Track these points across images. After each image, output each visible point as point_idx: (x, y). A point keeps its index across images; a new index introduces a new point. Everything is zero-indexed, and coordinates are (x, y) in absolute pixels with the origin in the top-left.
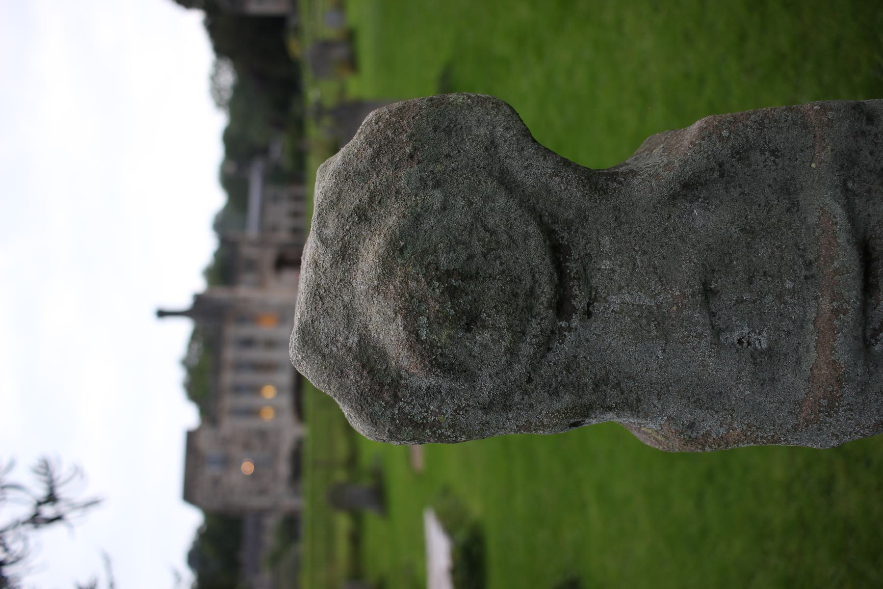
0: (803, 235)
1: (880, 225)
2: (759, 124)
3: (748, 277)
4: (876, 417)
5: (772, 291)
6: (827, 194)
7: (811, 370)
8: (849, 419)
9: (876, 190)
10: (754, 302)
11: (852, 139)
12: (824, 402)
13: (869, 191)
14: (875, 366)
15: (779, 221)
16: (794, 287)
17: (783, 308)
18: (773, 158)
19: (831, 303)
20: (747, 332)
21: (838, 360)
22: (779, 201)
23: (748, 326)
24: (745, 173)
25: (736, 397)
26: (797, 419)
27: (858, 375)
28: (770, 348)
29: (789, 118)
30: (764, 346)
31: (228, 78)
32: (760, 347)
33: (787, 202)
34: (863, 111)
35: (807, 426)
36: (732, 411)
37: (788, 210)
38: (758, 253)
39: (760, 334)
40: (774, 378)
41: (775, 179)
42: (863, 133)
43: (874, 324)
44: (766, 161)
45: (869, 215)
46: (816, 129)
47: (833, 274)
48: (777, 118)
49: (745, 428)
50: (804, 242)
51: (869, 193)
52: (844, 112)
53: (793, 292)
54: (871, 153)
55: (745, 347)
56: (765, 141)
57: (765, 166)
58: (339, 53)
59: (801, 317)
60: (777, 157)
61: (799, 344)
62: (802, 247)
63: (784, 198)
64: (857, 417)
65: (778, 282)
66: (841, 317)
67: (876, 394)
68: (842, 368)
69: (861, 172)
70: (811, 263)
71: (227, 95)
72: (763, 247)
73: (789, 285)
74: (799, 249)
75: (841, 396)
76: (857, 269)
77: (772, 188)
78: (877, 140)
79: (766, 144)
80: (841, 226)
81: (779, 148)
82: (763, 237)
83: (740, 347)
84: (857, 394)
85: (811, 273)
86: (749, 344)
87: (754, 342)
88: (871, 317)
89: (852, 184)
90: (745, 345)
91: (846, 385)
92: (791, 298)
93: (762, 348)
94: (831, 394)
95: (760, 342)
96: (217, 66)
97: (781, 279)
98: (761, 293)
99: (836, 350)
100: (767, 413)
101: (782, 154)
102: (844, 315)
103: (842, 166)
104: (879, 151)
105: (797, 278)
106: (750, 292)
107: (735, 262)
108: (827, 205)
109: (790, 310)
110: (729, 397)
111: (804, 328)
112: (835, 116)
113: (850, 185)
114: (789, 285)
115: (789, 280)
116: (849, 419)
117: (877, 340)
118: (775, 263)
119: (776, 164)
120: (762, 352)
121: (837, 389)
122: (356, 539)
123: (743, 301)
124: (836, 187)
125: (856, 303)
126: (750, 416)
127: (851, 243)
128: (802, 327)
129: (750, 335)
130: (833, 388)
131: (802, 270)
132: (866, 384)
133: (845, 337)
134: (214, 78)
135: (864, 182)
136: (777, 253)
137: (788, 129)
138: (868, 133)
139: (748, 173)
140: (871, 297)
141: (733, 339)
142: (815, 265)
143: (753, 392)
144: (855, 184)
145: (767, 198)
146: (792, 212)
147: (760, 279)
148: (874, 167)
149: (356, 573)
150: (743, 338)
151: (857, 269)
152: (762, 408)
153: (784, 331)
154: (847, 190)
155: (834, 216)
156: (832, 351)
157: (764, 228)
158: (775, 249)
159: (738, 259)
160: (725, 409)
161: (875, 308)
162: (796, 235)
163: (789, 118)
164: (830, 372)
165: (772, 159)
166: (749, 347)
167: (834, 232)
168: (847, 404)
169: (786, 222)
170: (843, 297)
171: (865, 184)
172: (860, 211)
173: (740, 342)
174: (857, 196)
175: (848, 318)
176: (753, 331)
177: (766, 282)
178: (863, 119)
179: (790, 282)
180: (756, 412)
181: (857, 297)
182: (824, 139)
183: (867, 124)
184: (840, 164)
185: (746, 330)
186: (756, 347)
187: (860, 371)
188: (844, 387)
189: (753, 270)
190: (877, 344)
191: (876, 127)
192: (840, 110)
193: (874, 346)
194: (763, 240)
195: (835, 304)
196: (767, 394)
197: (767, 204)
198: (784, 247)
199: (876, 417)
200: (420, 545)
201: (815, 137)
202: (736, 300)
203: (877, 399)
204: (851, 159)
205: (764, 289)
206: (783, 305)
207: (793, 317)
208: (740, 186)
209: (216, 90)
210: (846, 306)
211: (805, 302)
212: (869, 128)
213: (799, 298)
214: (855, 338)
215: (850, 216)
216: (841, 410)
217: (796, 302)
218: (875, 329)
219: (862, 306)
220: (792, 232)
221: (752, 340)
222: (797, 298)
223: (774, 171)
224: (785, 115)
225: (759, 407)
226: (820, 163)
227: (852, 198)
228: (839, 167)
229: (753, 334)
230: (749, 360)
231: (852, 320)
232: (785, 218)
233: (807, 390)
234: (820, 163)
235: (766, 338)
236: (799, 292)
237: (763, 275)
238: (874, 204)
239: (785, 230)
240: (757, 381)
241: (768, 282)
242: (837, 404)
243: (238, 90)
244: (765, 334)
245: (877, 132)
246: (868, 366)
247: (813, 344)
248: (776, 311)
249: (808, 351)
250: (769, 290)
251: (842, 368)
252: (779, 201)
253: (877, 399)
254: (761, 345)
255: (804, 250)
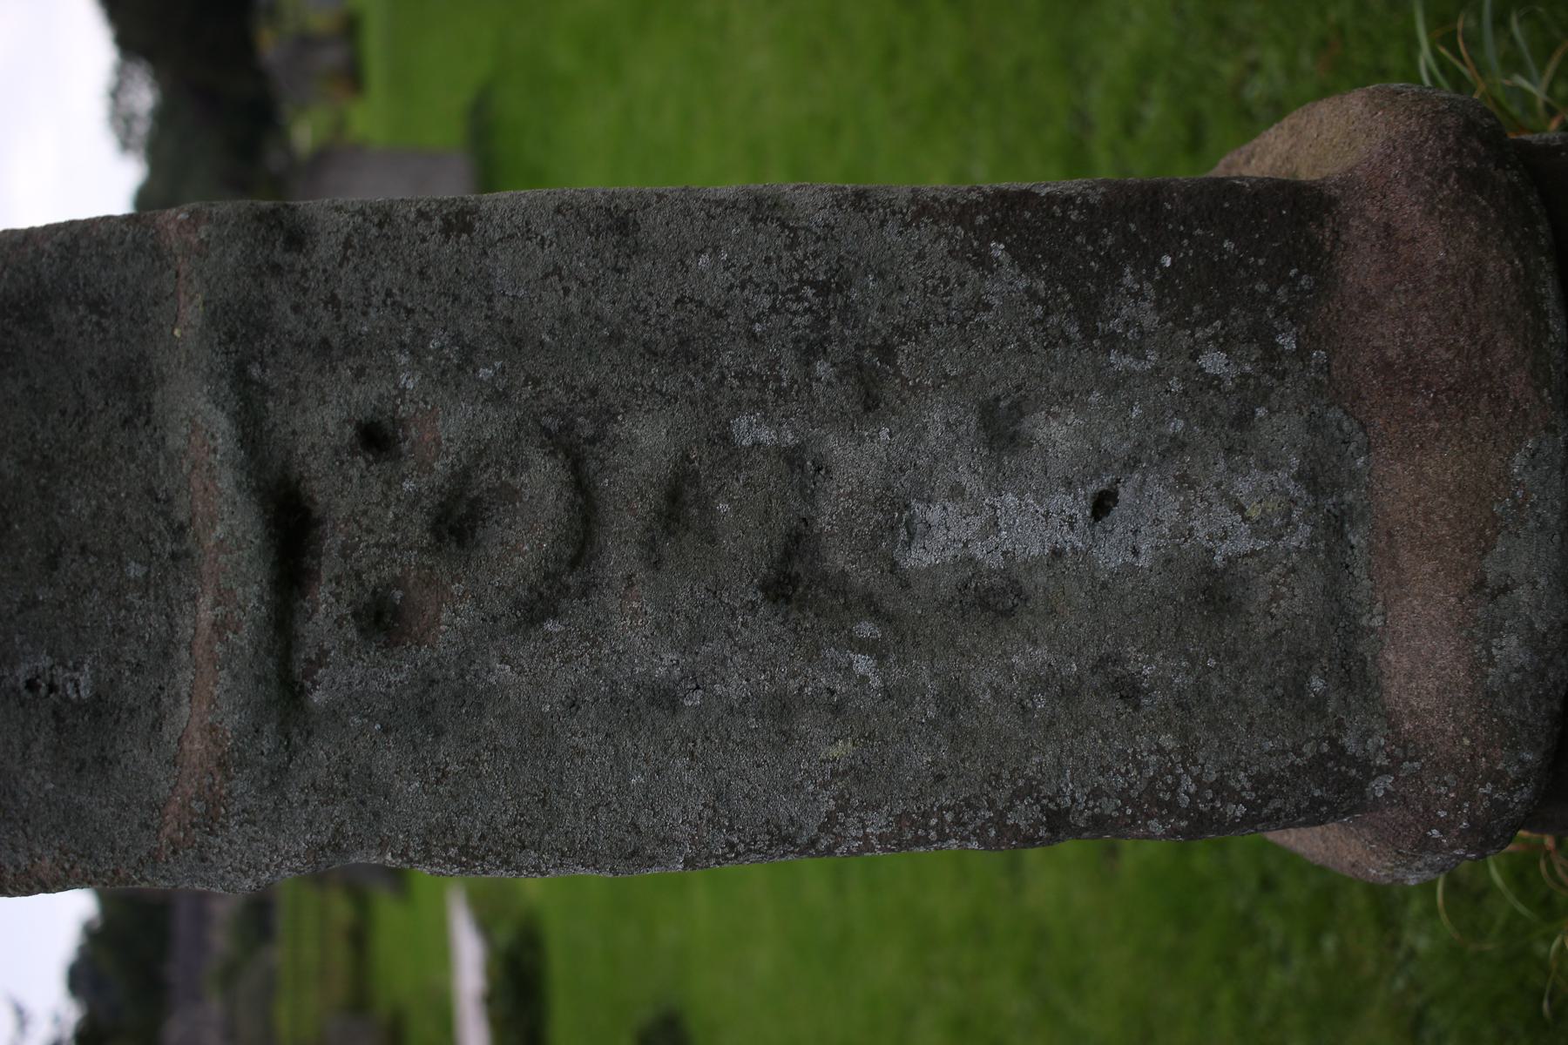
0: (161, 473)
1: (316, 453)
2: (67, 249)
3: (45, 555)
4: (308, 837)
5: (100, 584)
6: (201, 390)
7: (180, 741)
8: (253, 839)
9: (309, 383)
10: (61, 605)
11: (249, 280)
12: (197, 807)
13: (294, 385)
14: (305, 734)
15: (106, 443)
16: (147, 575)
17: (125, 617)
18: (95, 318)
19: (213, 609)
20: (47, 665)
21: (220, 723)
22: (107, 404)
23: (50, 653)
24: (38, 347)
25: (28, 794)
26: (157, 839)
27: (262, 753)
28: (98, 697)
29: (129, 237)
30: (85, 694)
31: (144, 98)
32: (74, 696)
33: (125, 406)
34: (281, 223)
35: (175, 852)
36: (24, 822)
37: (126, 422)
38: (70, 508)
39: (76, 669)
40: (105, 758)
41: (104, 359)
42: (276, 269)
43: (307, 650)
44: (81, 323)
45: (294, 433)
46: (180, 259)
47: (215, 550)
48: (105, 237)
49: (57, 855)
50: (167, 484)
51: (296, 388)
52: (233, 225)
53: (145, 586)
54: (296, 309)
55: (43, 695)
56: (77, 284)
57: (81, 334)
58: (331, 57)
59: (164, 635)
60: (103, 314)
61: (161, 688)
62: (162, 496)
63: (120, 398)
64: (268, 835)
65: (113, 566)
66: (228, 638)
67: (302, 790)
68: (228, 739)
69: (278, 346)
70: (182, 528)
71: (142, 128)
72: (78, 497)
73: (135, 570)
74: (157, 500)
75: (230, 792)
76: (257, 542)
77: (97, 377)
78: (305, 282)
79: (79, 288)
80: (224, 454)
81: (106, 297)
82: (76, 475)
83: (29, 696)
84: (261, 790)
85: (184, 548)
86: (52, 688)
87: (64, 686)
88: (303, 635)
89: (259, 371)
90: (43, 691)
91: (237, 773)
92: (140, 598)
93: (79, 697)
94: (210, 790)
95: (77, 686)
96: (121, 73)
97: (119, 560)
98: (75, 587)
99: (218, 702)
100: (98, 824)
101: (113, 310)
102: (235, 632)
103: (232, 337)
104: (313, 304)
105: (154, 558)
106: (51, 585)
107: (17, 526)
108: (199, 412)
109: (140, 621)
110: (14, 796)
111: (172, 657)
112: (214, 234)
113: (255, 371)
114: (135, 570)
115: (136, 561)
116: (253, 839)
117: (314, 683)
118: (105, 527)
119: (105, 330)
120: (80, 706)
121: (220, 782)
122: (359, 938)
123: (36, 603)
124: (221, 376)
125: (258, 609)
126: (63, 832)
127: (244, 491)
128: (166, 655)
129: (54, 672)
130: (214, 779)
131: (166, 540)
132: (283, 770)
133: (235, 677)
134: (116, 94)
135: (286, 366)
136: (111, 508)
137: (125, 260)
138: (286, 268)
139: (45, 348)
140: (303, 596)
141: (17, 679)
142: (190, 531)
143: (63, 786)
144: (268, 370)
145: (83, 397)
146: (135, 426)
147: (73, 561)
148: (306, 336)
149: (359, 1001)
150: (38, 677)
151: (257, 542)
152: (86, 817)
153: (128, 663)
154: (249, 382)
155: (213, 436)
156: (210, 706)
157: (74, 457)
158: (106, 501)
159: (21, 521)
160: (10, 819)
161: (309, 619)
162: (147, 473)
163: (129, 237)
164: (206, 747)
165: (94, 320)
166: (52, 696)
167: (211, 468)
168: (243, 811)
169: (122, 447)
170: (235, 596)
171: (288, 370)
172: (275, 425)
173: (31, 685)
174: (272, 394)
175: (241, 639)
176: (59, 664)
177: (85, 566)
178: (276, 240)
179: (138, 566)
180: (73, 824)
181: (261, 598)
182: (191, 281)
183: (286, 250)
184: (225, 329)
185: (45, 662)
186: (67, 695)
187: (266, 745)
188: (233, 778)
189: (56, 541)
190: (315, 689)
191: (305, 256)
192: (226, 223)
193: (311, 694)
194: (76, 482)
195: (219, 609)
196: (92, 789)
197: (81, 411)
198: (123, 495)
199: (308, 837)
200: (443, 954)
201: (177, 275)
202: (22, 603)
203: (306, 802)
204: (252, 319)
205: (82, 579)
206: (123, 612)
207: (147, 635)
208: (26, 374)
209: (121, 121)
210: (238, 615)
211: (170, 606)
212: (288, 258)
213: (157, 598)
214: (258, 680)
215: (245, 435)
216: (232, 823)
217: (152, 605)
218: (309, 661)
219: (273, 616)
220: (137, 466)
221: (59, 682)
222: (153, 598)
223: (100, 342)
224: (122, 231)
225: (79, 815)
226: (185, 328)
227: (259, 397)
228: (223, 337)
229: (60, 670)
230: (47, 722)
231: (251, 643)
232: (118, 438)
233: (172, 782)
234: (185, 328)
235: (88, 676)
236: (158, 585)
237: (79, 551)
238: (304, 411)
239: (121, 462)
240: (67, 763)
241: (90, 565)
242: (223, 811)
243: (163, 116)
244: (86, 668)
245: (308, 266)
246: (287, 736)
247: (185, 690)
248: (109, 624)
249: (177, 702)
250: (94, 582)
251: (228, 739)
252: (107, 404)
253: (306, 802)
254: (78, 692)
255: (169, 500)
